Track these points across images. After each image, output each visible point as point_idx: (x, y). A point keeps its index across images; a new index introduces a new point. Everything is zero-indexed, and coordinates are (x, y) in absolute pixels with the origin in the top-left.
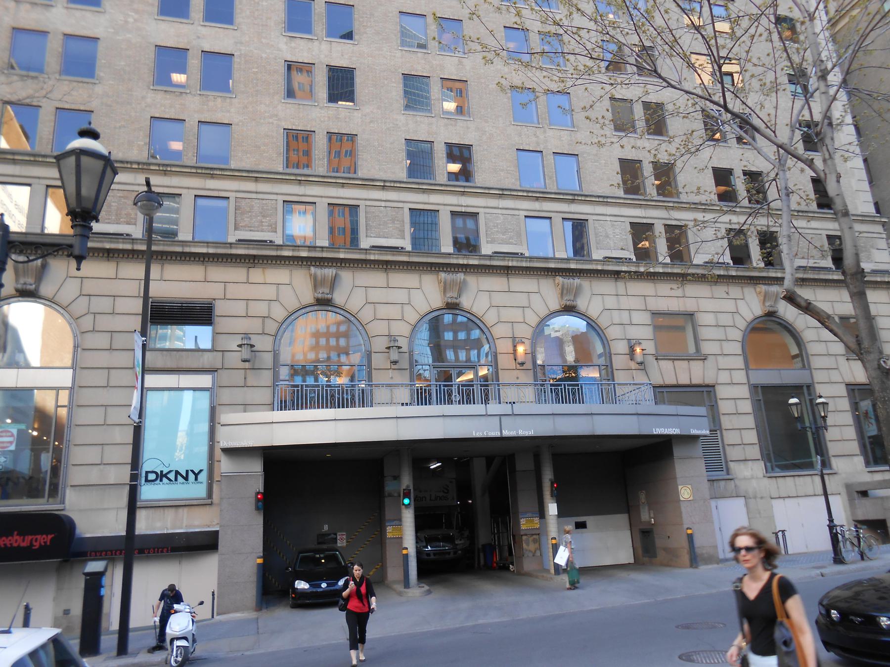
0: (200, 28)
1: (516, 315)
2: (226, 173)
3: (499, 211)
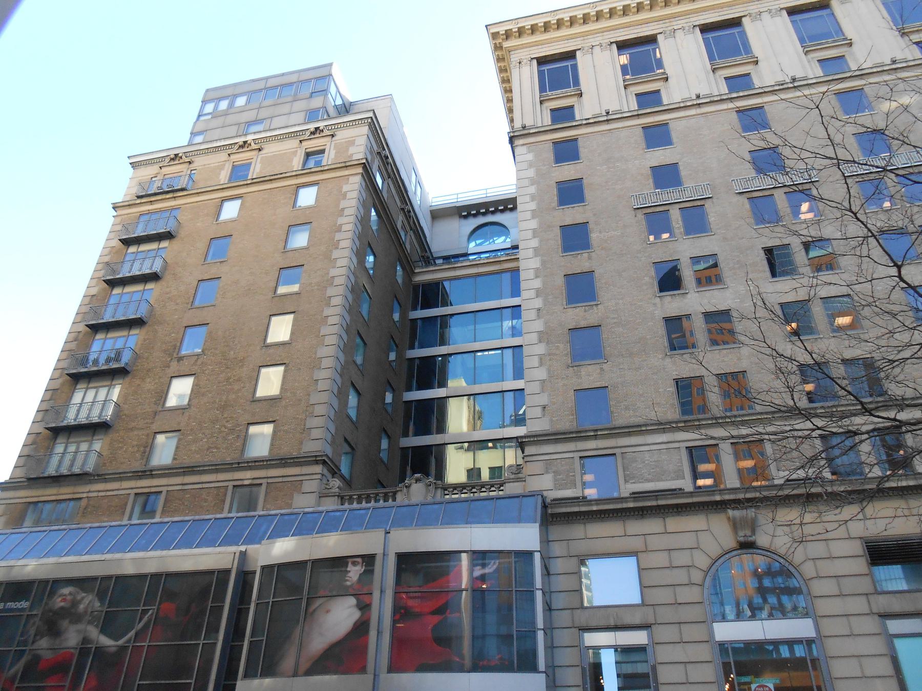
2: (582, 435)
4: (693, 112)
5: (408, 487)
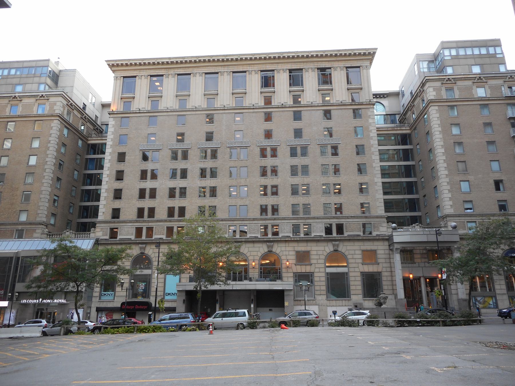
1: (255, 253)
3: (253, 224)
4: (165, 114)
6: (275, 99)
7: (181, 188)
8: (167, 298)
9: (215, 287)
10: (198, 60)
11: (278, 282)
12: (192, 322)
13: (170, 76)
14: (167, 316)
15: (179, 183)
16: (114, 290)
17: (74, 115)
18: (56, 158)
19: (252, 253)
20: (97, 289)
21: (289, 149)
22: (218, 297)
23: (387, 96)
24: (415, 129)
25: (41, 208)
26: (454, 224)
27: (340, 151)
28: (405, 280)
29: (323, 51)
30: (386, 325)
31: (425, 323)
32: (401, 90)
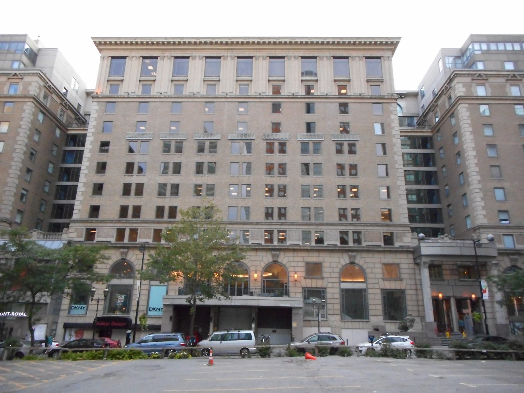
0: (171, 176)
1: (258, 263)
5: (31, 233)
6: (284, 89)
7: (172, 185)
8: (151, 313)
9: (208, 302)
10: (198, 42)
11: (285, 298)
12: (182, 345)
13: (166, 59)
14: (150, 337)
15: (172, 179)
16: (86, 303)
17: (53, 100)
18: (26, 146)
19: (255, 263)
20: (66, 302)
21: (299, 144)
22: (212, 315)
23: (404, 97)
24: (437, 132)
25: (5, 202)
26: (490, 236)
27: (358, 148)
28: (436, 301)
29: (341, 37)
30: (441, 357)
31: (492, 355)
32: (420, 91)
